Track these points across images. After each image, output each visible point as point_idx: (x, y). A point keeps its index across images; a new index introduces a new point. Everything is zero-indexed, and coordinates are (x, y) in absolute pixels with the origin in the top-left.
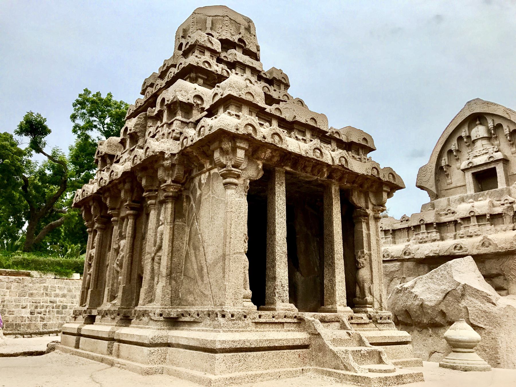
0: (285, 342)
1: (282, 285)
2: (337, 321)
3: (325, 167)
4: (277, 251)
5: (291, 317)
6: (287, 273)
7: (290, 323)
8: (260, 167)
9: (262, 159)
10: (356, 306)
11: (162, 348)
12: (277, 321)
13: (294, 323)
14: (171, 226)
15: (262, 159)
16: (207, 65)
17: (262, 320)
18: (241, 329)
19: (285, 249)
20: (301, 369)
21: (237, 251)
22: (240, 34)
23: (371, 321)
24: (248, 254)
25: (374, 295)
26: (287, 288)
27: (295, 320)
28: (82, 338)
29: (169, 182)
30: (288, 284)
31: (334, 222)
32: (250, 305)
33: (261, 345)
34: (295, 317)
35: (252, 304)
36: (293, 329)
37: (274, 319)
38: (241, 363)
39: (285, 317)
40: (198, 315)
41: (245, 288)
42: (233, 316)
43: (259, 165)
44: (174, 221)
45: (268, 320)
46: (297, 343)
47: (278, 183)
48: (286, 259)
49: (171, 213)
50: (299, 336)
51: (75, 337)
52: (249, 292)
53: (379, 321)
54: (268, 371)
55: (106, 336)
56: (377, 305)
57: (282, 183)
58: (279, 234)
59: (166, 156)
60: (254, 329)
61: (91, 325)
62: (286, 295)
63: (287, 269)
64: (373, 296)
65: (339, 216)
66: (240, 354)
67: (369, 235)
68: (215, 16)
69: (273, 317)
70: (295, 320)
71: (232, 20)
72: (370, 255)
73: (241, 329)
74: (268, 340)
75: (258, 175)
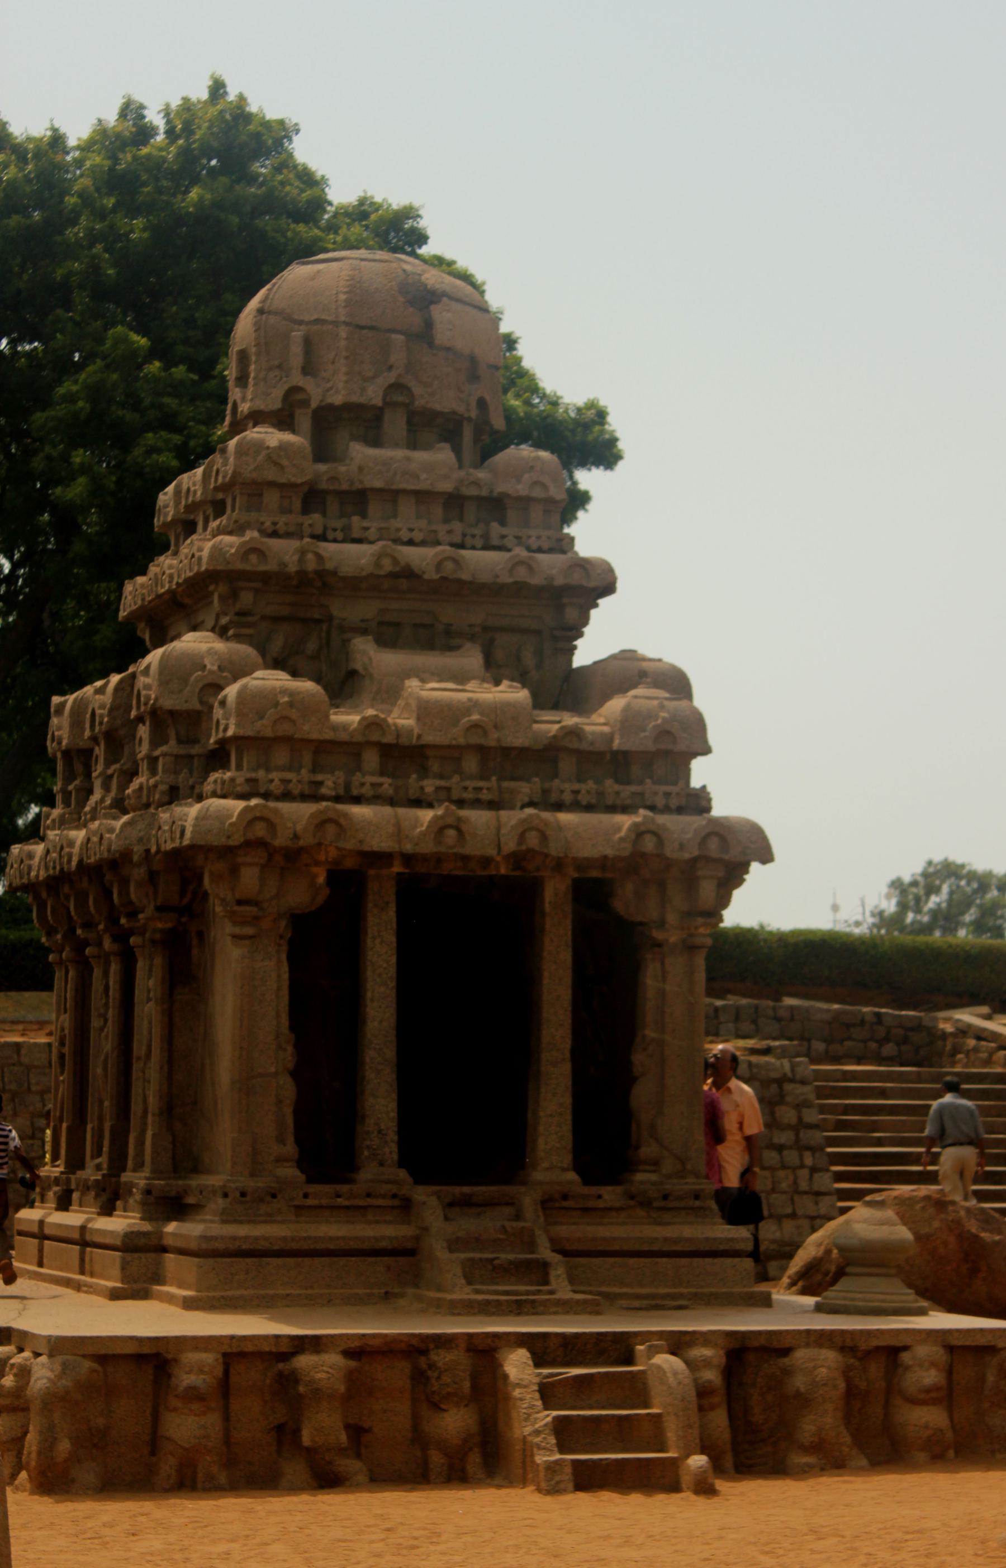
2: (507, 1204)
4: (368, 1060)
6: (394, 1105)
7: (379, 1207)
8: (321, 879)
10: (641, 1167)
11: (148, 1255)
12: (347, 1203)
13: (393, 1207)
16: (253, 558)
17: (309, 1202)
18: (261, 1218)
20: (383, 1291)
22: (390, 368)
26: (393, 1136)
27: (396, 1202)
28: (46, 1242)
29: (150, 911)
30: (396, 1129)
31: (546, 974)
33: (294, 1246)
34: (395, 1196)
35: (299, 1173)
37: (339, 1200)
39: (369, 1195)
40: (201, 1192)
41: (281, 1140)
42: (243, 1194)
45: (324, 1202)
46: (384, 1244)
48: (394, 1076)
50: (389, 1231)
51: (36, 1241)
52: (290, 1148)
53: (656, 1204)
54: (310, 1291)
55: (193, 1246)
56: (668, 1166)
57: (387, 903)
58: (376, 1024)
59: (135, 858)
60: (293, 1218)
61: (65, 1214)
62: (391, 1151)
65: (566, 956)
66: (249, 1260)
68: (317, 321)
69: (339, 1196)
70: (396, 1202)
71: (362, 328)
73: (261, 1218)
74: (309, 1238)
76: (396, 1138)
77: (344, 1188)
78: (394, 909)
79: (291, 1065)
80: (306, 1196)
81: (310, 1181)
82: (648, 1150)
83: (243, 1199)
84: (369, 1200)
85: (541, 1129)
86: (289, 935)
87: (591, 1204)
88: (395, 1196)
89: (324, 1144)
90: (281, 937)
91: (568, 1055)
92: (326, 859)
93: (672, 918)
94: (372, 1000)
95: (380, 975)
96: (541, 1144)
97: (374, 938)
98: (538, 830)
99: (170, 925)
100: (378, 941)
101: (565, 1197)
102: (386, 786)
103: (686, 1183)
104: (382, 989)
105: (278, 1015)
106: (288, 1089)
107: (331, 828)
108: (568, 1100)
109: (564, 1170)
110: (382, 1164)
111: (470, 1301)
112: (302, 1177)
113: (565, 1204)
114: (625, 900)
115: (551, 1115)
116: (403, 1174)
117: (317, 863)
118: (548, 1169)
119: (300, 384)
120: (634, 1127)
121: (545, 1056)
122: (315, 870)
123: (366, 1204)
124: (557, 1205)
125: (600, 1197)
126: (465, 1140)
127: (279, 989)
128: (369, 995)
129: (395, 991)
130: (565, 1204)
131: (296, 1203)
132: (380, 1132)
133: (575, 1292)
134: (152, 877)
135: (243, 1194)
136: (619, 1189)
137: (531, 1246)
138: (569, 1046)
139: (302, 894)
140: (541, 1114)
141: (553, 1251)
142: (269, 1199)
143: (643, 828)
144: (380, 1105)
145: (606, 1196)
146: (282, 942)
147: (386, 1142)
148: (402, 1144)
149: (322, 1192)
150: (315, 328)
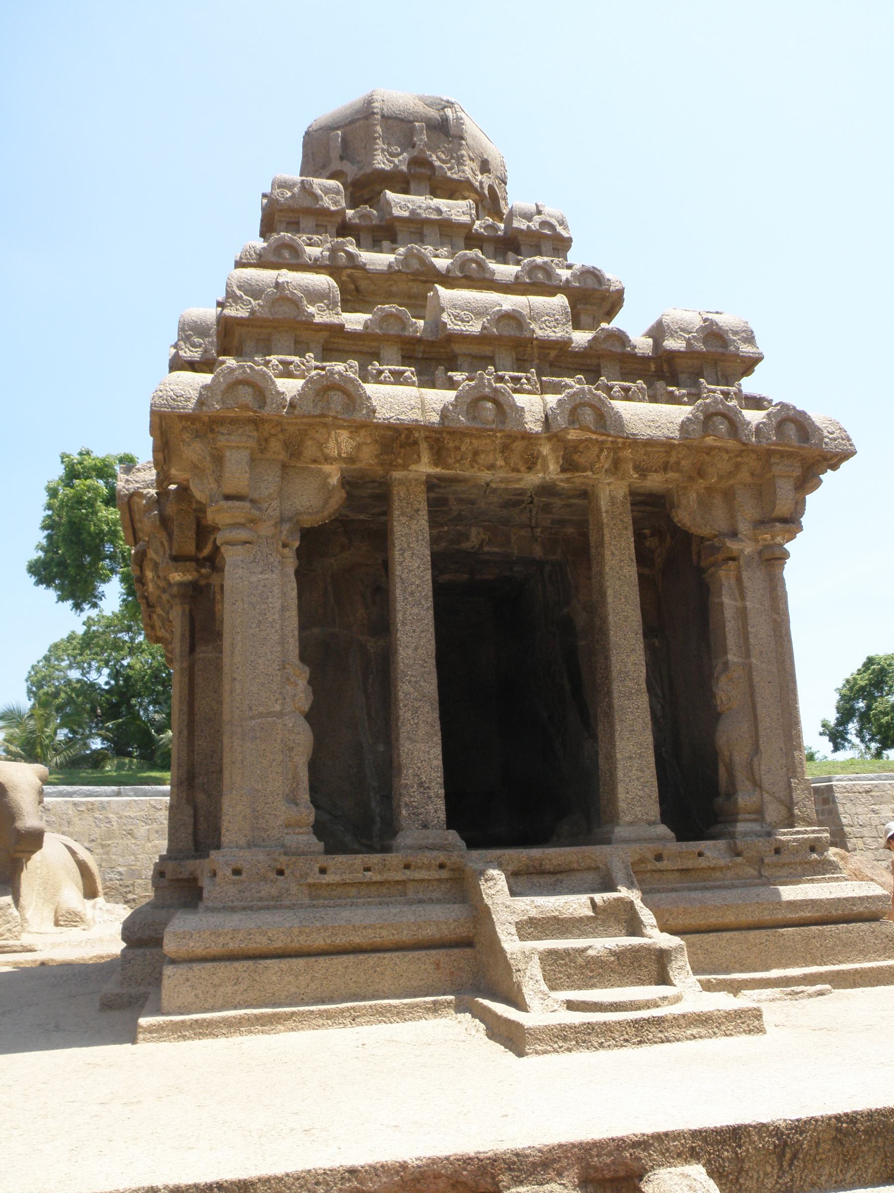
0: (384, 933)
1: (421, 784)
2: (589, 869)
3: (542, 442)
4: (401, 695)
5: (429, 867)
6: (438, 751)
7: (422, 880)
8: (334, 480)
9: (335, 459)
12: (378, 878)
14: (185, 665)
15: (335, 459)
17: (327, 878)
19: (431, 687)
21: (261, 709)
23: (739, 860)
24: (309, 717)
25: (766, 785)
26: (438, 790)
27: (444, 874)
31: (609, 592)
32: (309, 840)
34: (442, 866)
35: (314, 839)
36: (434, 895)
38: (242, 987)
39: (407, 867)
42: (237, 872)
43: (329, 476)
44: (192, 649)
45: (348, 877)
47: (403, 514)
48: (436, 715)
49: (183, 635)
57: (417, 511)
62: (437, 809)
63: (438, 739)
64: (761, 788)
65: (631, 571)
67: (743, 613)
69: (367, 869)
72: (749, 669)
75: (326, 502)
76: (442, 792)
77: (374, 859)
78: (426, 518)
79: (306, 708)
80: (323, 871)
81: (329, 851)
82: (745, 799)
83: (237, 878)
84: (407, 872)
85: (620, 774)
86: (297, 544)
87: (689, 864)
88: (442, 866)
89: (351, 809)
90: (285, 546)
91: (644, 686)
92: (339, 455)
93: (744, 527)
94: (404, 624)
95: (412, 594)
96: (621, 794)
97: (403, 550)
98: (592, 406)
99: (189, 577)
100: (407, 554)
101: (659, 858)
102: (407, 374)
103: (798, 833)
104: (415, 610)
105: (282, 641)
106: (303, 738)
107: (337, 398)
108: (648, 738)
109: (651, 823)
110: (425, 826)
111: (563, 1028)
112: (321, 846)
113: (659, 865)
114: (686, 515)
115: (630, 758)
116: (453, 836)
117: (328, 459)
118: (631, 824)
119: (339, 168)
120: (722, 771)
121: (617, 687)
122: (327, 468)
123: (404, 878)
124: (650, 867)
125: (700, 854)
126: (524, 790)
127: (283, 609)
128: (400, 616)
129: (431, 612)
130: (659, 865)
131: (310, 880)
132: (421, 784)
133: (708, 987)
134: (165, 522)
135: (237, 872)
136: (721, 844)
137: (634, 927)
138: (643, 675)
139: (315, 495)
140: (618, 756)
141: (662, 931)
142: (273, 875)
143: (711, 410)
144: (421, 754)
145: (708, 853)
146: (286, 550)
147: (430, 798)
148: (450, 798)
149: (346, 867)
150: (349, 128)
